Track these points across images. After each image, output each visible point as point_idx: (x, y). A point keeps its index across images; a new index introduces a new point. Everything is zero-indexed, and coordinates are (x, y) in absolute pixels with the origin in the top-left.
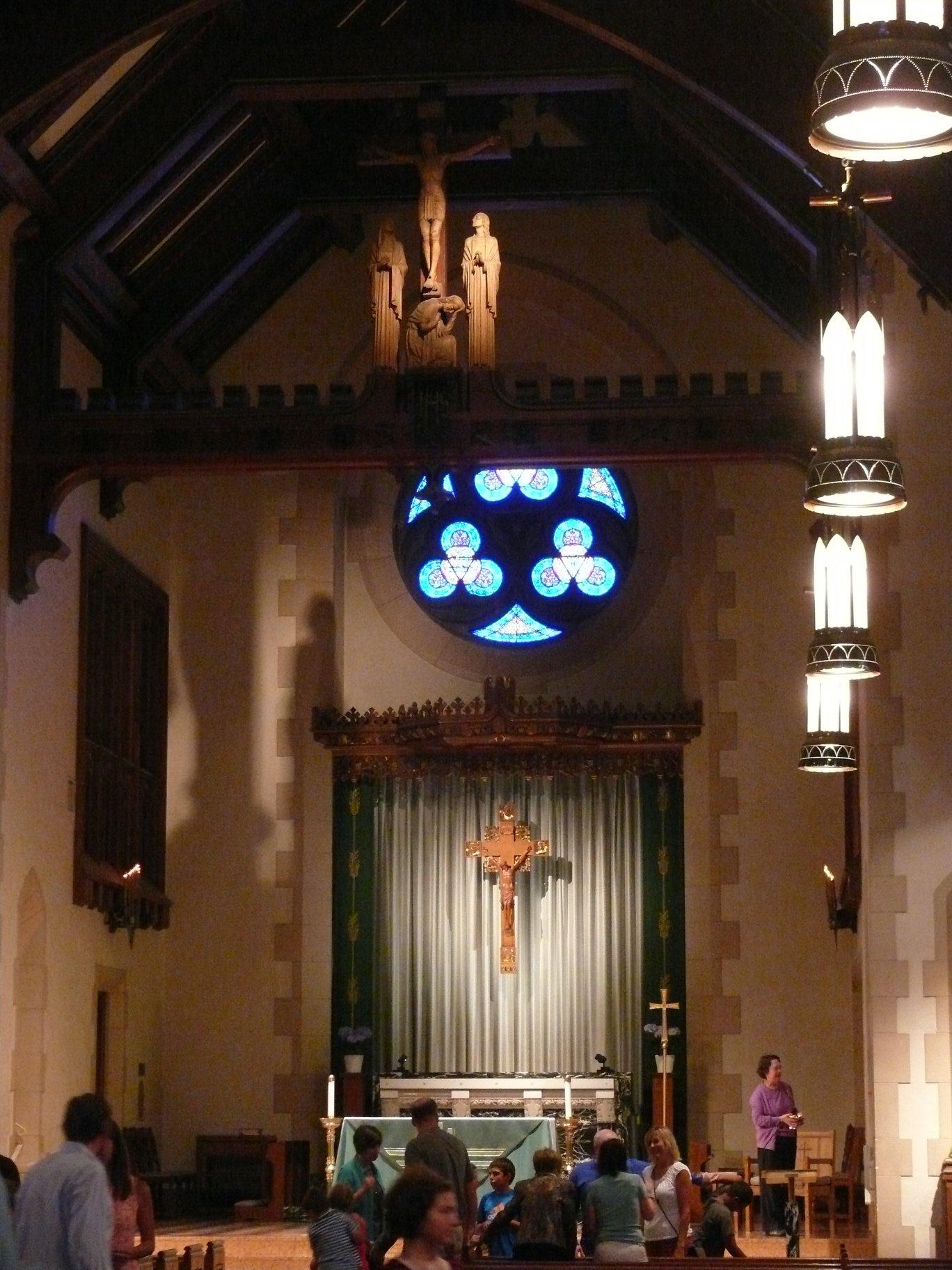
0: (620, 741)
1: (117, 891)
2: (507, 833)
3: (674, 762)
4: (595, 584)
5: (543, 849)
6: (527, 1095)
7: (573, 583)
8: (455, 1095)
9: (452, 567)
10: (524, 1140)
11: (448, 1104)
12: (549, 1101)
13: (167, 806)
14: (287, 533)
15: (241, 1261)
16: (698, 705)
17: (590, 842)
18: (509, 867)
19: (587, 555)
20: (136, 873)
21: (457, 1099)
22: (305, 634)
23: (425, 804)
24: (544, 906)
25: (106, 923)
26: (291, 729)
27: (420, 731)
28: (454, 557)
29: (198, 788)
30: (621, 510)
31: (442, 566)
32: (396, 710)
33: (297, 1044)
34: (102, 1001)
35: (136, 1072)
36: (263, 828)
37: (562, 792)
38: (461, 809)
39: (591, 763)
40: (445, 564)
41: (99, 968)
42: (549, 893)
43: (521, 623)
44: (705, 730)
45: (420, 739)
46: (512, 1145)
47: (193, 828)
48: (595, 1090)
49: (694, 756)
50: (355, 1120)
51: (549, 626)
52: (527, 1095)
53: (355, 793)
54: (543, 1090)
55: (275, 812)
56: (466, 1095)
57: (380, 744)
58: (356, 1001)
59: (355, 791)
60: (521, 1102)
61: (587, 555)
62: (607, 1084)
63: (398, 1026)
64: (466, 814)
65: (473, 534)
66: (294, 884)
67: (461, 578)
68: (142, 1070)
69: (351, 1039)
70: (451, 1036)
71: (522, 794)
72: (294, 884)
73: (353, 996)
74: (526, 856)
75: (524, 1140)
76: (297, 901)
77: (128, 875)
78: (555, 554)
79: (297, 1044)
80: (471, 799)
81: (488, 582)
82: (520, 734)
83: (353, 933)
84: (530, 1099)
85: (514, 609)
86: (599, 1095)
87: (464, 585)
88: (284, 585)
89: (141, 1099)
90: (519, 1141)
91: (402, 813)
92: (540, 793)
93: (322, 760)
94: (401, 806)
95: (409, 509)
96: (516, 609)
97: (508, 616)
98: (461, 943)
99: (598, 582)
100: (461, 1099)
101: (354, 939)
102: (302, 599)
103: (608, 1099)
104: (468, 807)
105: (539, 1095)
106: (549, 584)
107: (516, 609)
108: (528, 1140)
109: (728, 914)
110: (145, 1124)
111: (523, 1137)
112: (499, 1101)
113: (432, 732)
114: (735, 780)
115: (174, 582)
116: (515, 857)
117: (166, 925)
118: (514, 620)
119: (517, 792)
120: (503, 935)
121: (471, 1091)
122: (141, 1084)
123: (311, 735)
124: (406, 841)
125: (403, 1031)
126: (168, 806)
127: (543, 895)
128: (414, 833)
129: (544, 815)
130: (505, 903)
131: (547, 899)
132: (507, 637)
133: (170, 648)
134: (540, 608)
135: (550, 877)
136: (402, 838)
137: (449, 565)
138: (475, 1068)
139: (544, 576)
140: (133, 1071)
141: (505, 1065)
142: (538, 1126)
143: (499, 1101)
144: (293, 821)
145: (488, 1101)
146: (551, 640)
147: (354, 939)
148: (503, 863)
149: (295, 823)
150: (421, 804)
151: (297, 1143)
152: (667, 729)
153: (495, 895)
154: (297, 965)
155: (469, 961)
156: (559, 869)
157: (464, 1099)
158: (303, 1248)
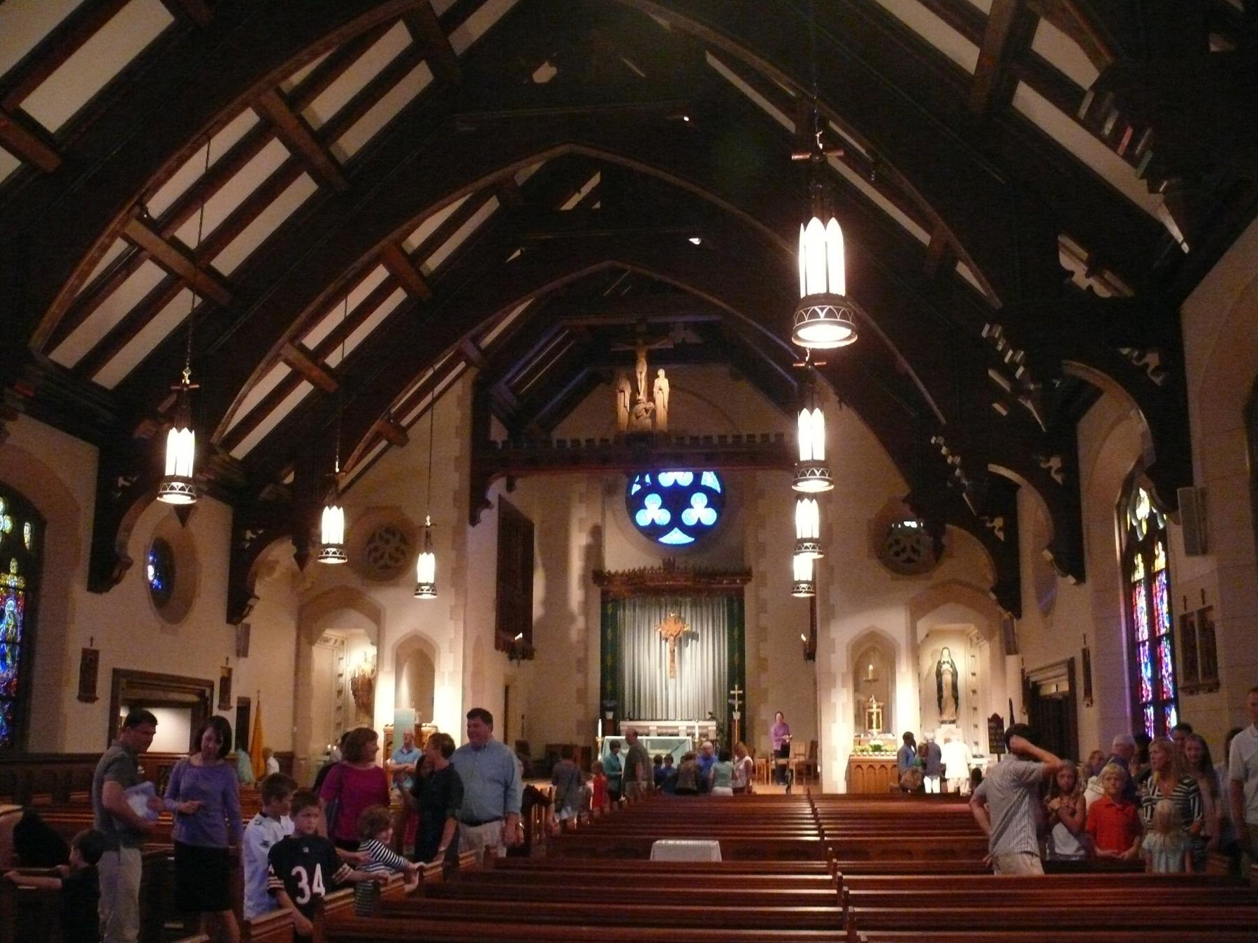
16: (750, 569)
29: (547, 602)
32: (627, 571)
33: (586, 706)
36: (571, 618)
37: (694, 605)
41: (506, 676)
49: (749, 590)
53: (610, 605)
68: (523, 717)
76: (586, 649)
88: (581, 520)
92: (686, 605)
94: (629, 610)
102: (589, 526)
128: (634, 621)
129: (687, 614)
150: (637, 610)
153: (667, 647)
154: (586, 675)
156: (694, 636)
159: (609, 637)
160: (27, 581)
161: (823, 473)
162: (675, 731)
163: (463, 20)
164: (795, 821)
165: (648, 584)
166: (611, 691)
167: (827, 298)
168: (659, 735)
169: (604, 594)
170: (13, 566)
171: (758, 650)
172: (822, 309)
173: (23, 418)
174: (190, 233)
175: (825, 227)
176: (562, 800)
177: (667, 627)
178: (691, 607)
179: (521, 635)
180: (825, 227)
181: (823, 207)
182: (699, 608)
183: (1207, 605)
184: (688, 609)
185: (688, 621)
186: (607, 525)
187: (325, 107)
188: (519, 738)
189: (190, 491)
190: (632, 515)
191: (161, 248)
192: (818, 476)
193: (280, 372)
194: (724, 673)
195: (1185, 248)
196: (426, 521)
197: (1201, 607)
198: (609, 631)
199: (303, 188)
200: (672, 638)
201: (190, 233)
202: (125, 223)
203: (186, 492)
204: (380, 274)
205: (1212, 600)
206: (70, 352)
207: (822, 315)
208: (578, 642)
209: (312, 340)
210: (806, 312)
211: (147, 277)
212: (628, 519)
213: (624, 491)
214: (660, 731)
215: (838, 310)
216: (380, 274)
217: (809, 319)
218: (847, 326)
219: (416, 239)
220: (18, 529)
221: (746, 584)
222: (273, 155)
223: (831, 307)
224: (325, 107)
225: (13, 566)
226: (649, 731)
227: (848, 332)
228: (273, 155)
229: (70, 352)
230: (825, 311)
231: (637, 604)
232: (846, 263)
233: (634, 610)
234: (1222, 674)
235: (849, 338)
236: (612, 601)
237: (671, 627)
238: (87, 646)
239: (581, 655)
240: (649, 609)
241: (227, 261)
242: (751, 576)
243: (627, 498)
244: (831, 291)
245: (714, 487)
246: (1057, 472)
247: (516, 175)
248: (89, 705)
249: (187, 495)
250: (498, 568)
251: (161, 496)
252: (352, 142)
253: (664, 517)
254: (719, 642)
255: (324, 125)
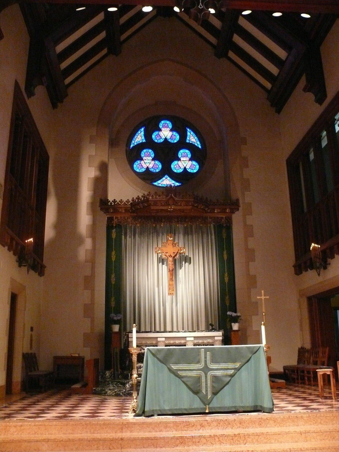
0: (210, 212)
1: (24, 247)
2: (170, 244)
3: (229, 221)
4: (192, 169)
5: (183, 250)
6: (188, 339)
7: (185, 169)
8: (159, 339)
9: (145, 163)
10: (251, 357)
11: (156, 343)
12: (196, 341)
13: (46, 223)
14: (92, 140)
15: (89, 441)
16: (238, 200)
17: (197, 250)
18: (172, 256)
19: (189, 160)
20: (31, 241)
21: (160, 341)
22: (98, 173)
23: (138, 237)
24: (181, 273)
25: (17, 261)
26: (92, 205)
27: (141, 205)
28: (146, 160)
29: (57, 226)
30: (200, 147)
31: (141, 162)
32: (130, 200)
33: (92, 321)
34: (14, 298)
35: (30, 330)
36: (80, 241)
37: (187, 233)
38: (151, 238)
39: (200, 220)
40: (142, 162)
41: (13, 281)
42: (183, 268)
43: (168, 181)
44: (241, 209)
45: (140, 209)
46: (245, 361)
47: (53, 241)
48: (214, 336)
49: (237, 218)
50: (153, 349)
51: (177, 182)
52: (188, 339)
53: (114, 230)
54: (194, 337)
55: (85, 234)
56: (164, 339)
57: (124, 212)
58: (114, 306)
59: (114, 230)
60: (185, 342)
61: (189, 160)
62: (219, 334)
63: (129, 317)
64: (153, 239)
65: (152, 153)
66: (92, 262)
67: (148, 166)
68: (32, 329)
69: (115, 318)
70: (148, 320)
71: (173, 233)
72: (92, 262)
73: (113, 304)
74: (177, 253)
75: (251, 357)
76: (93, 268)
77: (28, 242)
78: (179, 159)
79: (92, 321)
80: (155, 235)
81: (157, 168)
82: (179, 205)
83: (113, 281)
84: (189, 341)
85: (165, 176)
86: (216, 338)
87: (171, 129)
88: (90, 157)
89: (31, 340)
90: (249, 358)
91: (130, 239)
92: (179, 233)
93: (103, 218)
94: (130, 237)
95: (130, 145)
96: (166, 176)
97: (164, 178)
98: (152, 285)
99: (193, 169)
100: (161, 341)
101: (113, 283)
102: (97, 162)
103: (220, 340)
104: (154, 237)
105: (192, 339)
106: (177, 169)
107: (166, 176)
108: (252, 357)
109: (252, 272)
110: (32, 351)
111: (250, 356)
112: (176, 342)
113: (146, 205)
114: (252, 225)
115: (52, 153)
116: (173, 253)
117: (43, 275)
118: (166, 180)
119: (173, 232)
120: (169, 281)
121: (165, 338)
122: (31, 336)
123: (99, 208)
124: (131, 251)
125: (130, 317)
126: (45, 233)
127: (181, 269)
128: (135, 245)
129: (181, 240)
130: (170, 269)
131: (183, 270)
132: (163, 185)
133: (49, 177)
134: (174, 176)
135: (183, 262)
136: (130, 251)
137: (144, 162)
138: (158, 329)
139: (175, 166)
140: (28, 332)
141: (169, 328)
142: (259, 348)
143: (176, 342)
144: (92, 238)
145: (172, 342)
146: (178, 186)
147: (113, 283)
148: (169, 255)
149: (93, 239)
150: (137, 236)
151: (96, 359)
152: (228, 208)
153: (164, 269)
154: (93, 290)
155: (155, 291)
156: (187, 260)
157: (163, 341)
158: (127, 428)
159: (113, 259)
162: (183, 342)
163: (3, 200)
164: (95, 405)
165: (152, 208)
168: (166, 346)
169: (110, 220)
171: (248, 270)
176: (164, 439)
177: (165, 249)
178: (184, 236)
179: (31, 240)
182: (190, 236)
184: (181, 236)
185: (181, 245)
186: (110, 163)
188: (26, 350)
190: (131, 163)
194: (189, 301)
198: (113, 253)
200: (171, 259)
208: (86, 261)
212: (128, 167)
213: (125, 145)
214: (167, 342)
221: (234, 213)
226: (158, 342)
231: (137, 231)
233: (134, 236)
236: (116, 226)
237: (170, 250)
239: (88, 272)
240: (148, 238)
242: (239, 206)
243: (126, 150)
250: (13, 108)
253: (156, 166)
254: (209, 265)
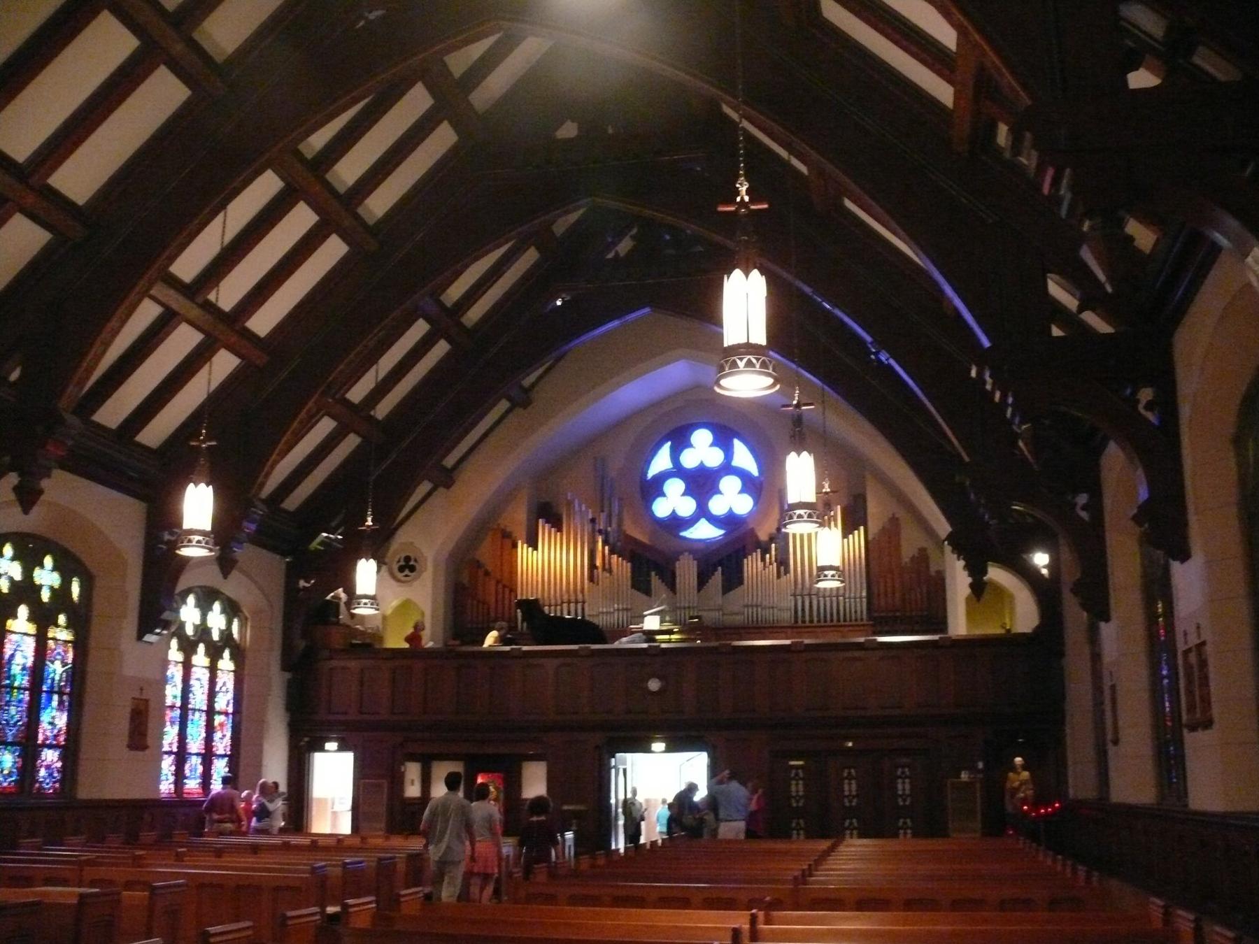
160: (76, 635)
161: (810, 516)
166: (1014, 788)
167: (749, 348)
170: (62, 619)
172: (741, 359)
173: (58, 474)
174: (228, 294)
175: (747, 277)
180: (747, 277)
181: (747, 260)
183: (1202, 640)
187: (348, 171)
189: (207, 543)
191: (195, 312)
192: (805, 518)
193: (325, 426)
195: (1109, 289)
196: (1157, 609)
197: (1198, 642)
199: (333, 250)
201: (228, 294)
202: (151, 285)
203: (837, 578)
204: (420, 328)
205: (1207, 635)
206: (113, 413)
207: (741, 364)
209: (357, 394)
210: (727, 362)
211: (184, 339)
215: (758, 360)
216: (420, 328)
217: (730, 369)
218: (769, 375)
219: (455, 292)
220: (66, 585)
222: (301, 219)
223: (751, 357)
224: (348, 171)
225: (62, 619)
227: (770, 381)
228: (301, 219)
229: (113, 413)
230: (745, 360)
232: (767, 315)
234: (1216, 711)
235: (773, 385)
238: (137, 695)
241: (263, 322)
244: (750, 341)
245: (691, 530)
246: (1084, 508)
247: (555, 225)
248: (140, 753)
249: (202, 547)
251: (179, 549)
252: (379, 204)
255: (349, 189)
